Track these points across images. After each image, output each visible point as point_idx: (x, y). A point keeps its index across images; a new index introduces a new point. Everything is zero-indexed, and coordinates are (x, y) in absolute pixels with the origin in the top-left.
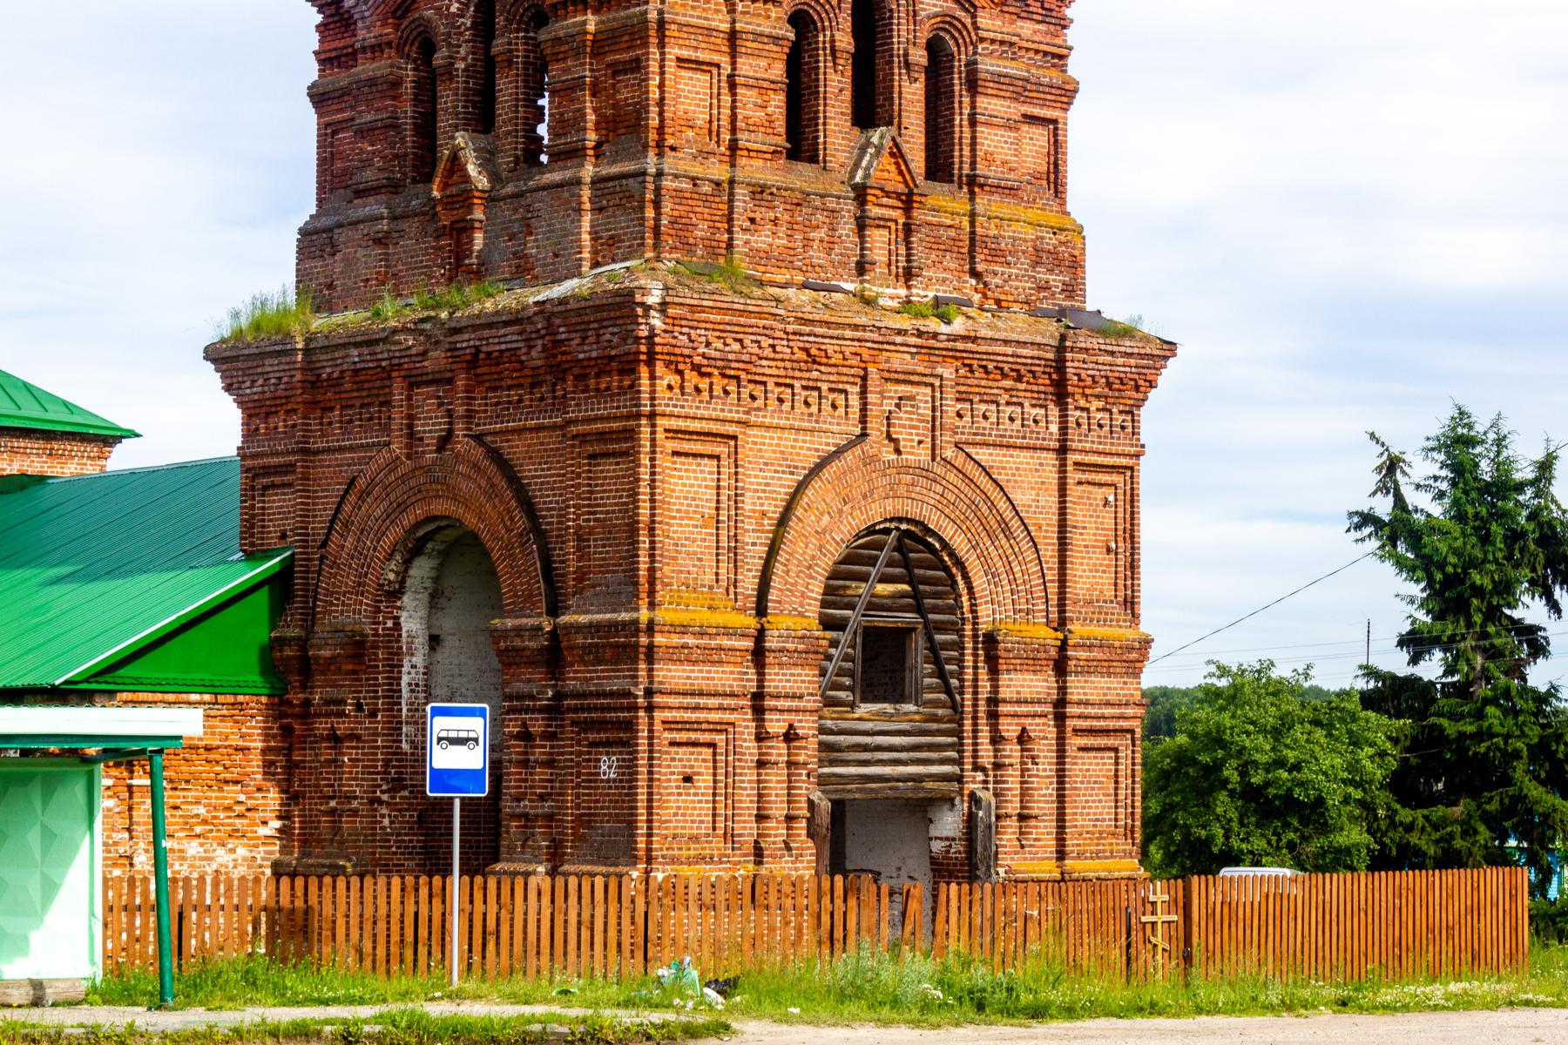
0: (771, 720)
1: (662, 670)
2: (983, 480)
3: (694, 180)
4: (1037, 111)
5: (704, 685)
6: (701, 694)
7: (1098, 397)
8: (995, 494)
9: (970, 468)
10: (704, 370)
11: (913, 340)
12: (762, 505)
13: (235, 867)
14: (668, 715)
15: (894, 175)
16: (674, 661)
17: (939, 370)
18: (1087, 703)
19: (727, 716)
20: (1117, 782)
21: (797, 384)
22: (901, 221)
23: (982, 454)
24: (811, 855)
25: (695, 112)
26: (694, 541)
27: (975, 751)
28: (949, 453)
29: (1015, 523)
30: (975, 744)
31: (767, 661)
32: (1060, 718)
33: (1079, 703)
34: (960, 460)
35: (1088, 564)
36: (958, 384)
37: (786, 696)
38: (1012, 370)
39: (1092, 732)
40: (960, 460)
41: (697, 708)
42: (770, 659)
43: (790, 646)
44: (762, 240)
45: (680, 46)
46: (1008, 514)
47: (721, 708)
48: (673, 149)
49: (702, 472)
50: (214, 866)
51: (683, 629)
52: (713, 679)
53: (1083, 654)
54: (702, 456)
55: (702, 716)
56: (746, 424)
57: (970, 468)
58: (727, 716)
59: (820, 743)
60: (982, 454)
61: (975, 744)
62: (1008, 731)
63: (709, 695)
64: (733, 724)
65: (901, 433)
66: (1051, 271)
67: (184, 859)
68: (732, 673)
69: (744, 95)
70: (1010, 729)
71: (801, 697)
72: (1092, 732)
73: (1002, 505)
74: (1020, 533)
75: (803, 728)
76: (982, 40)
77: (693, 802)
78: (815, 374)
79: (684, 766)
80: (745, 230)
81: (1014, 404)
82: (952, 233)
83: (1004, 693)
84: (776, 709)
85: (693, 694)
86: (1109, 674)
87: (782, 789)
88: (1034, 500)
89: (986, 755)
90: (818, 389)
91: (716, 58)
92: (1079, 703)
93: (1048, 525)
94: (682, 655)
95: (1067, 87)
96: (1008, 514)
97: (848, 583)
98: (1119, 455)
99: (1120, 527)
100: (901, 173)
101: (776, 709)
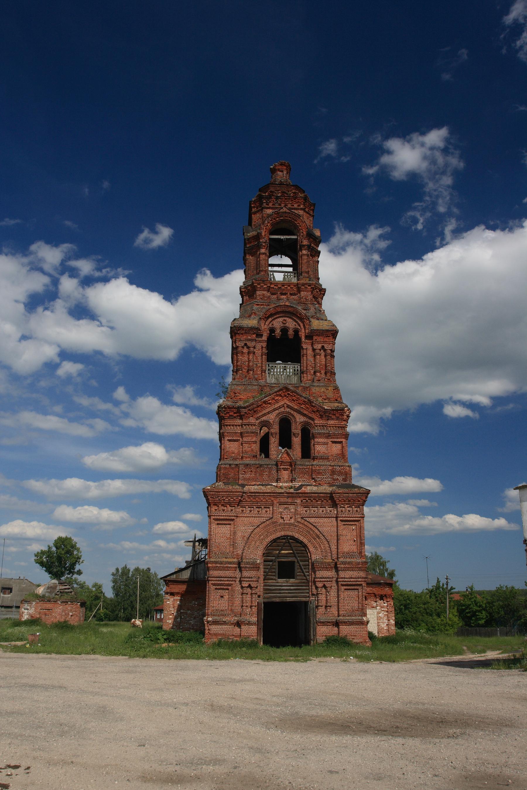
0: (244, 583)
1: (212, 572)
2: (310, 526)
3: (230, 465)
4: (335, 440)
5: (223, 575)
6: (221, 577)
7: (347, 504)
8: (314, 529)
9: (306, 523)
10: (225, 505)
11: (286, 495)
12: (244, 534)
13: (199, 616)
14: (213, 582)
15: (288, 459)
16: (215, 570)
17: (296, 501)
18: (344, 578)
19: (230, 582)
20: (358, 598)
21: (254, 507)
22: (291, 468)
23: (312, 520)
24: (256, 615)
25: (234, 450)
26: (224, 543)
27: (312, 590)
28: (299, 520)
29: (321, 535)
30: (312, 588)
31: (242, 570)
32: (337, 582)
33: (342, 578)
34: (303, 521)
35: (348, 544)
36: (301, 504)
37: (247, 578)
38: (347, 499)
39: (218, 585)
40: (303, 521)
41: (221, 581)
42: (243, 569)
43: (248, 566)
44: (247, 476)
45: (229, 437)
46: (318, 533)
47: (228, 581)
48: (226, 459)
49: (227, 528)
50: (194, 616)
51: (216, 562)
52: (226, 574)
53: (342, 566)
54: (227, 524)
55: (223, 582)
56: (237, 517)
57: (306, 523)
58: (230, 582)
59: (264, 588)
60: (312, 520)
61: (312, 588)
62: (319, 585)
63: (224, 578)
64: (232, 584)
65: (284, 516)
66: (339, 476)
67: (187, 614)
68: (232, 572)
69: (245, 445)
70: (320, 585)
71: (252, 578)
72: (218, 585)
73: (316, 531)
74: (322, 538)
75: (253, 585)
76: (316, 426)
77: (223, 602)
78: (259, 504)
79: (221, 594)
80: (242, 474)
81: (323, 507)
82: (307, 470)
83: (317, 576)
84: (244, 581)
85: (219, 577)
86: (353, 571)
87: (250, 599)
88: (329, 530)
89: (315, 591)
90: (261, 508)
91: (239, 438)
92: (342, 578)
93: (334, 535)
94: (216, 569)
95: (343, 433)
96: (318, 533)
97: (273, 551)
98: (355, 517)
99: (358, 535)
100: (289, 458)
101: (244, 581)
